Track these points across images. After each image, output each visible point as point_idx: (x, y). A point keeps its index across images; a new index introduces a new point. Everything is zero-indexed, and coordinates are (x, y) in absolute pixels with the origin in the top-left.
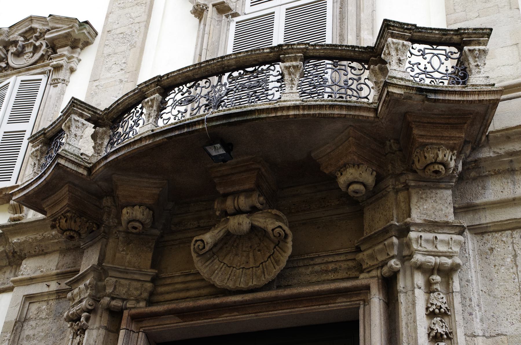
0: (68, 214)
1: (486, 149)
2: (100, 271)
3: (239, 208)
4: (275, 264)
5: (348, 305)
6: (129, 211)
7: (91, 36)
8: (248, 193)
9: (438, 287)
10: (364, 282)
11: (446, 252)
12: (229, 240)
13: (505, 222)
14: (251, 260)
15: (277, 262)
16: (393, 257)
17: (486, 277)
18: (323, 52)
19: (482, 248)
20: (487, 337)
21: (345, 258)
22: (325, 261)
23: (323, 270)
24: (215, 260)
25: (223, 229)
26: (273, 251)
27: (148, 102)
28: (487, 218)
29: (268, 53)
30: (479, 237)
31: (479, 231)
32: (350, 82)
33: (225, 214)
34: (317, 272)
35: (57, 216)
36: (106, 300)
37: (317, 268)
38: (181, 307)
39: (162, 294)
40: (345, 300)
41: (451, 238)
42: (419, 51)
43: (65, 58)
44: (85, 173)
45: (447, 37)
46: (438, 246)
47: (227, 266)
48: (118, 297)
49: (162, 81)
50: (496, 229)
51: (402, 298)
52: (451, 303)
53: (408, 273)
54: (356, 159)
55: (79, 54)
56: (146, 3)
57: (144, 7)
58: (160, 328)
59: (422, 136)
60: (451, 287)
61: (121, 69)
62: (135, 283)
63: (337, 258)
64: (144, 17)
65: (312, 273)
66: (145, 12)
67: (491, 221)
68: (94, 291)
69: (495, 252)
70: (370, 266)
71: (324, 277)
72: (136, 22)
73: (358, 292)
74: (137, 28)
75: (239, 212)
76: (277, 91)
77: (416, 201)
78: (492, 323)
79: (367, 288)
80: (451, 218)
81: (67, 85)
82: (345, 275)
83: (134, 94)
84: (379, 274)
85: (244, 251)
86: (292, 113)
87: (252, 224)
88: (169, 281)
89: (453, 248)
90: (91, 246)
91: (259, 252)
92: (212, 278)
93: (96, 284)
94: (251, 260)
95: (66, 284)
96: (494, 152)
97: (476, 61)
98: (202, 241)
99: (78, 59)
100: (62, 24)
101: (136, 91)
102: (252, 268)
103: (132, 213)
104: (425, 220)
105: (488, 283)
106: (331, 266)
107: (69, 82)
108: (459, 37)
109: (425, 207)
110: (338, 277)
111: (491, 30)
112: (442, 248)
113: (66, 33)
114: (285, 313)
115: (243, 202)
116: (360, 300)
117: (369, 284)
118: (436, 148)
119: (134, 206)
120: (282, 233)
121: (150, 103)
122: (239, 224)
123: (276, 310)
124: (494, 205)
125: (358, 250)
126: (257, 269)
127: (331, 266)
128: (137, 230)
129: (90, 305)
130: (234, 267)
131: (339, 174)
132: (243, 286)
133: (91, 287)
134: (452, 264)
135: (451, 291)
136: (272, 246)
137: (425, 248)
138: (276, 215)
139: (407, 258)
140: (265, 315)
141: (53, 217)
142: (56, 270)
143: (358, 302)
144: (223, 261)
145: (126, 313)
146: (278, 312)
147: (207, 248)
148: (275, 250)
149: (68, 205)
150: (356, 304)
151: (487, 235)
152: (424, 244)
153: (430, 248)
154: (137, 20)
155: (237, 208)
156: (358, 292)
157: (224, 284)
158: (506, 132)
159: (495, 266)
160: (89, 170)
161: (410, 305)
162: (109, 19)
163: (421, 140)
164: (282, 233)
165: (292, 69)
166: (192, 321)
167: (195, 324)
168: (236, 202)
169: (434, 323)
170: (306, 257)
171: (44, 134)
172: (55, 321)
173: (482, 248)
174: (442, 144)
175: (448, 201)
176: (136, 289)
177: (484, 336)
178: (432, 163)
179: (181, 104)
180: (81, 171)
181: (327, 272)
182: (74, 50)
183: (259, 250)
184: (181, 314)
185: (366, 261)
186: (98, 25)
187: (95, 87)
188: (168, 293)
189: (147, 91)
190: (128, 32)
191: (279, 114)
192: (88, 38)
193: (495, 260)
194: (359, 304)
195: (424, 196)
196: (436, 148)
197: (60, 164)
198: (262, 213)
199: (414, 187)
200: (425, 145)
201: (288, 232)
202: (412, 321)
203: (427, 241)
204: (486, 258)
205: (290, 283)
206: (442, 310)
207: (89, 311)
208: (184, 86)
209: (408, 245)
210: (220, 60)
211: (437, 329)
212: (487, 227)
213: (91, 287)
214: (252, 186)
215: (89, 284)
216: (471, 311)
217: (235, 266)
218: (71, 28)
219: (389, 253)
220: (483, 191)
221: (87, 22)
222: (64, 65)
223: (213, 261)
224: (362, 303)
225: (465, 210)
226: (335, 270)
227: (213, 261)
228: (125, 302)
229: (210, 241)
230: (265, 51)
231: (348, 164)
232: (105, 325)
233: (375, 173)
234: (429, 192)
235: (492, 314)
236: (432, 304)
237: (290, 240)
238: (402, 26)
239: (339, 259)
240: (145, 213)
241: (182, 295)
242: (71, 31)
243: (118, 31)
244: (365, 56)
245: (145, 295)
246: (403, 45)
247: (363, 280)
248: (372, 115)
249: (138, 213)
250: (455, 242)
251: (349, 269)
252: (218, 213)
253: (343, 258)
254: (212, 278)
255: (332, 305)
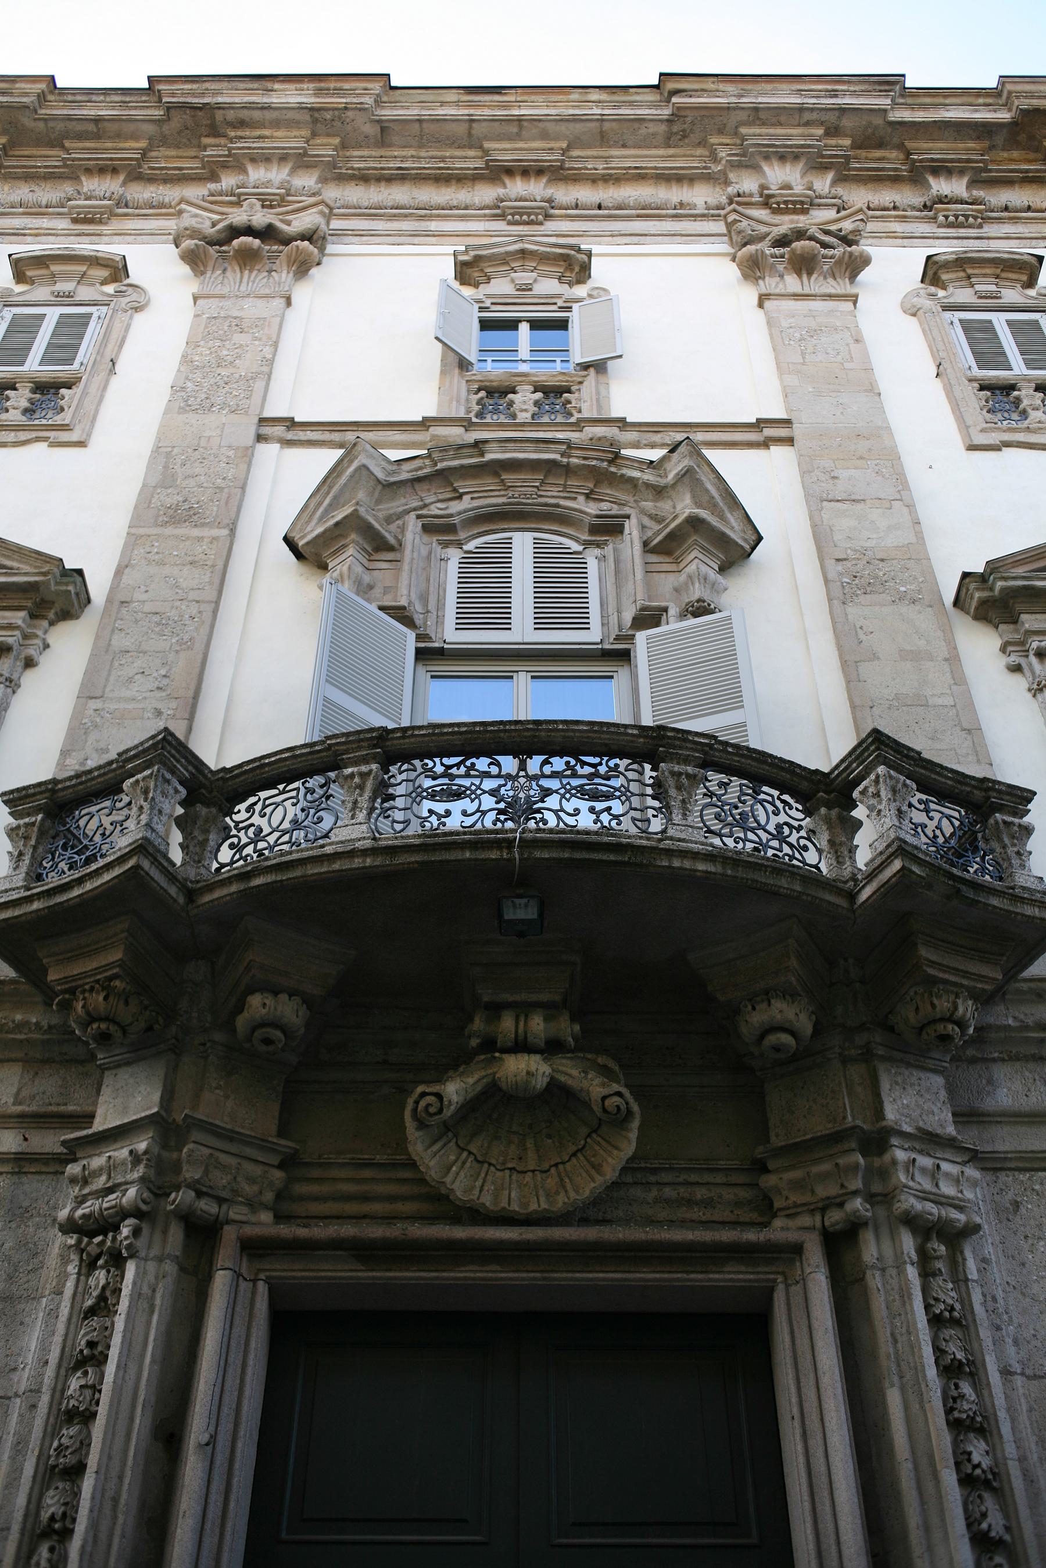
0: (117, 983)
1: (1001, 1008)
2: (165, 1126)
3: (526, 1038)
4: (593, 1172)
5: (750, 1280)
6: (268, 1002)
7: (79, 602)
8: (551, 1010)
9: (939, 1265)
10: (792, 1236)
11: (953, 1198)
12: (494, 1105)
13: (1040, 1155)
14: (531, 1155)
15: (597, 1168)
16: (855, 1193)
17: (1013, 1257)
18: (738, 762)
19: (997, 1198)
20: (1028, 1378)
21: (724, 1180)
22: (681, 1180)
23: (683, 1198)
24: (450, 1141)
25: (483, 1077)
26: (583, 1142)
27: (352, 776)
28: (1006, 1141)
29: (633, 735)
30: (990, 1177)
31: (989, 1165)
32: (786, 830)
33: (490, 1046)
34: (668, 1201)
35: (80, 982)
36: (181, 1197)
37: (668, 1192)
38: (371, 1235)
39: (302, 1198)
40: (743, 1268)
41: (962, 1172)
42: (920, 801)
43: (17, 633)
44: (181, 900)
45: (964, 788)
46: (941, 1184)
47: (476, 1159)
48: (210, 1191)
49: (388, 740)
50: (1021, 1165)
51: (875, 1281)
52: (966, 1301)
53: (884, 1230)
54: (795, 983)
55: (46, 632)
56: (213, 566)
57: (208, 574)
58: (308, 1278)
59: (933, 964)
60: (961, 1268)
61: (159, 688)
62: (249, 1167)
63: (707, 1178)
64: (210, 594)
65: (657, 1201)
66: (211, 583)
67: (1013, 1149)
68: (152, 1171)
69: (1023, 1210)
70: (796, 1206)
71: (683, 1213)
72: (190, 598)
73: (775, 1255)
74: (194, 612)
75: (522, 1046)
76: (654, 816)
77: (888, 1086)
78: (1035, 1350)
79: (797, 1250)
80: (951, 1130)
81: (14, 692)
82: (727, 1215)
83: (310, 753)
84: (818, 1224)
85: (514, 1133)
86: (701, 866)
87: (552, 1078)
88: (316, 1173)
89: (965, 1192)
90: (128, 1063)
91: (550, 1141)
92: (448, 1179)
93: (159, 1155)
94: (531, 1155)
95: (64, 1143)
96: (1015, 1018)
97: (1014, 845)
98: (439, 1096)
99: (44, 643)
100: (20, 562)
101: (317, 748)
102: (533, 1171)
103: (275, 1009)
104: (919, 1129)
105: (1018, 1270)
106: (700, 1193)
107: (19, 686)
108: (984, 794)
109: (905, 1102)
110: (714, 1218)
111: (1035, 793)
112: (948, 1189)
113: (29, 583)
114: (612, 1280)
115: (537, 1026)
116: (778, 1273)
117: (803, 1243)
118: (952, 992)
119: (276, 993)
120: (623, 1107)
121: (357, 780)
122: (528, 1073)
123: (591, 1272)
124: (1018, 1119)
125: (762, 1168)
126: (544, 1175)
127: (700, 1193)
128: (271, 1048)
129: (144, 1201)
130: (490, 1164)
131: (750, 1007)
132: (517, 1209)
133: (148, 1160)
134: (967, 1223)
135: (961, 1277)
136: (584, 1131)
137: (919, 1183)
138: (605, 1067)
139: (879, 1198)
140: (565, 1279)
141: (66, 983)
142: (14, 1104)
143: (772, 1276)
144: (469, 1148)
145: (229, 1235)
146: (596, 1275)
147: (448, 1113)
148: (589, 1140)
149: (121, 964)
150: (768, 1280)
151: (1004, 1173)
152: (918, 1177)
153: (927, 1185)
154: (192, 596)
155: (521, 1038)
156: (775, 1255)
157: (475, 1198)
158: (1039, 984)
159: (1026, 1237)
160: (191, 895)
161: (897, 1297)
162: (125, 577)
163: (931, 971)
164: (623, 1107)
165: (684, 780)
166: (390, 1270)
167: (395, 1278)
168: (522, 1024)
169: (944, 1340)
170: (643, 1165)
171: (53, 791)
172: (13, 1225)
173: (997, 1198)
174: (962, 986)
175: (942, 1099)
176: (251, 1180)
177: (1023, 1374)
178: (942, 1020)
179: (433, 796)
180: (173, 891)
181: (690, 1203)
182: (36, 622)
183: (549, 1136)
184: (364, 1251)
185: (785, 1193)
186: (98, 586)
187: (91, 712)
188: (316, 1199)
189: (347, 752)
190: (173, 614)
191: (676, 863)
192: (73, 605)
193: (1024, 1226)
194: (775, 1281)
195: (899, 1079)
196: (952, 992)
197: (143, 869)
198: (571, 1058)
199: (884, 1059)
200: (934, 981)
201: (635, 1107)
202: (904, 1330)
203: (923, 1170)
204: (1009, 1220)
205: (608, 1217)
206: (956, 1314)
207: (137, 1213)
208: (437, 760)
209: (884, 1173)
210: (530, 726)
211: (954, 1353)
212: (1006, 1158)
213: (148, 1160)
214: (558, 998)
215: (146, 1152)
216: (999, 1322)
217: (493, 1161)
218: (44, 574)
219: (846, 1184)
220: (989, 1088)
221: (80, 572)
222: (15, 648)
223: (445, 1145)
224: (780, 1279)
225: (965, 1119)
226: (708, 1203)
227: (445, 1145)
228: (225, 1207)
229: (455, 1098)
230: (630, 731)
231: (775, 991)
232: (178, 1253)
233: (814, 1017)
234: (907, 1072)
235: (1033, 1332)
236: (937, 1300)
237: (636, 1124)
238: (898, 747)
239: (712, 1180)
240: (300, 1013)
241: (350, 1208)
242: (43, 582)
243: (148, 608)
244: (804, 785)
245: (269, 1197)
246: (905, 785)
247: (780, 1230)
248: (843, 902)
249: (289, 1010)
250: (968, 1180)
251: (738, 1204)
252: (474, 1042)
253: (720, 1178)
254: (448, 1179)
255: (717, 1276)
